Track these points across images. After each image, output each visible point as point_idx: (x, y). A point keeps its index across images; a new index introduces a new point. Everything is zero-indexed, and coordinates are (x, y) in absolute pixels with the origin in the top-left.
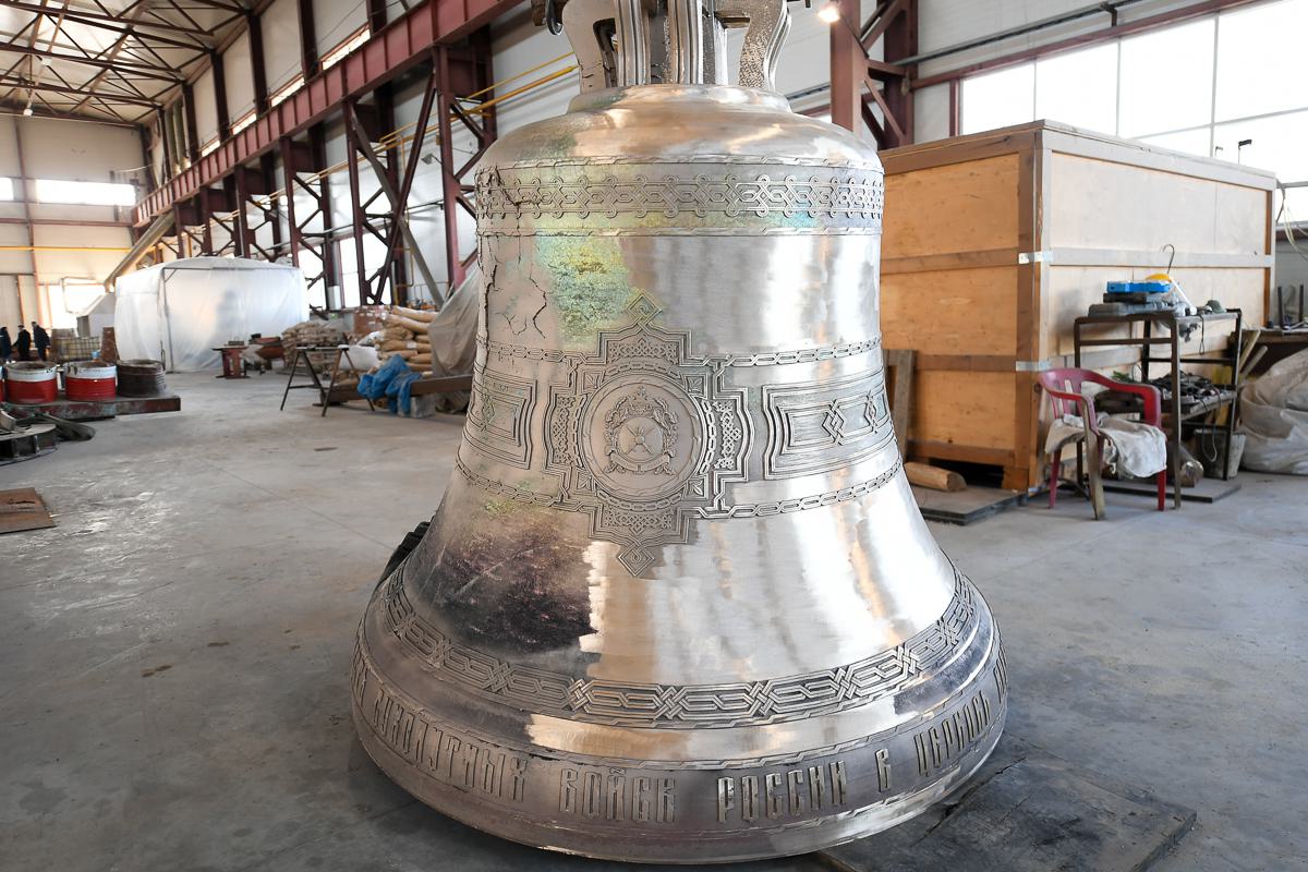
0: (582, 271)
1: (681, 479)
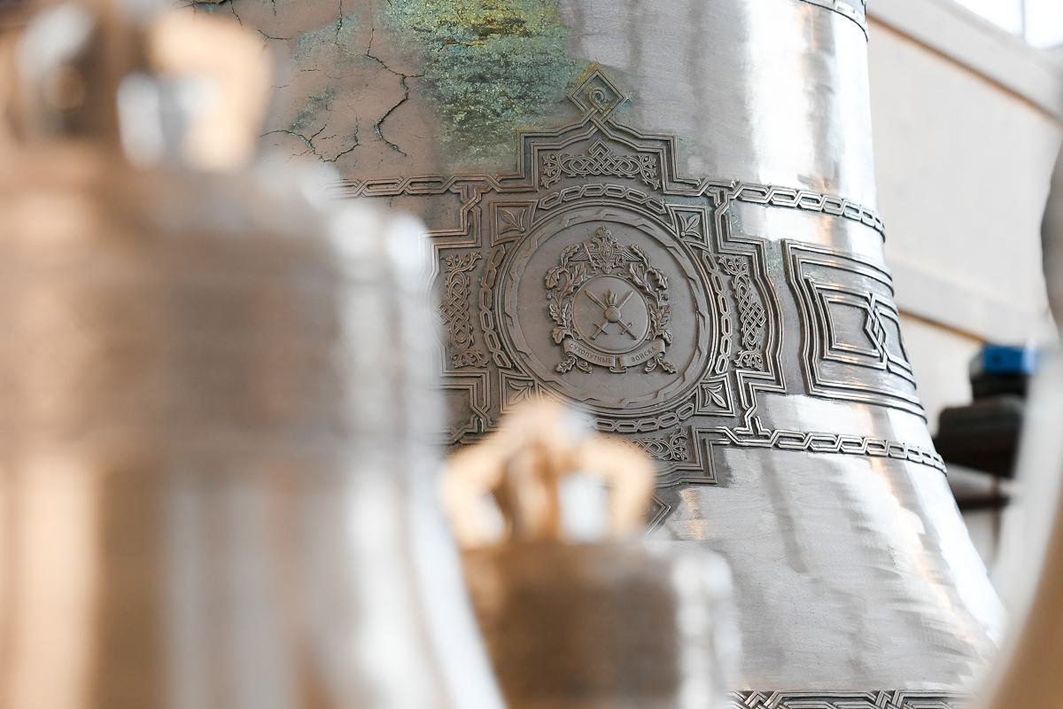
0: (484, 34)
1: (688, 382)
